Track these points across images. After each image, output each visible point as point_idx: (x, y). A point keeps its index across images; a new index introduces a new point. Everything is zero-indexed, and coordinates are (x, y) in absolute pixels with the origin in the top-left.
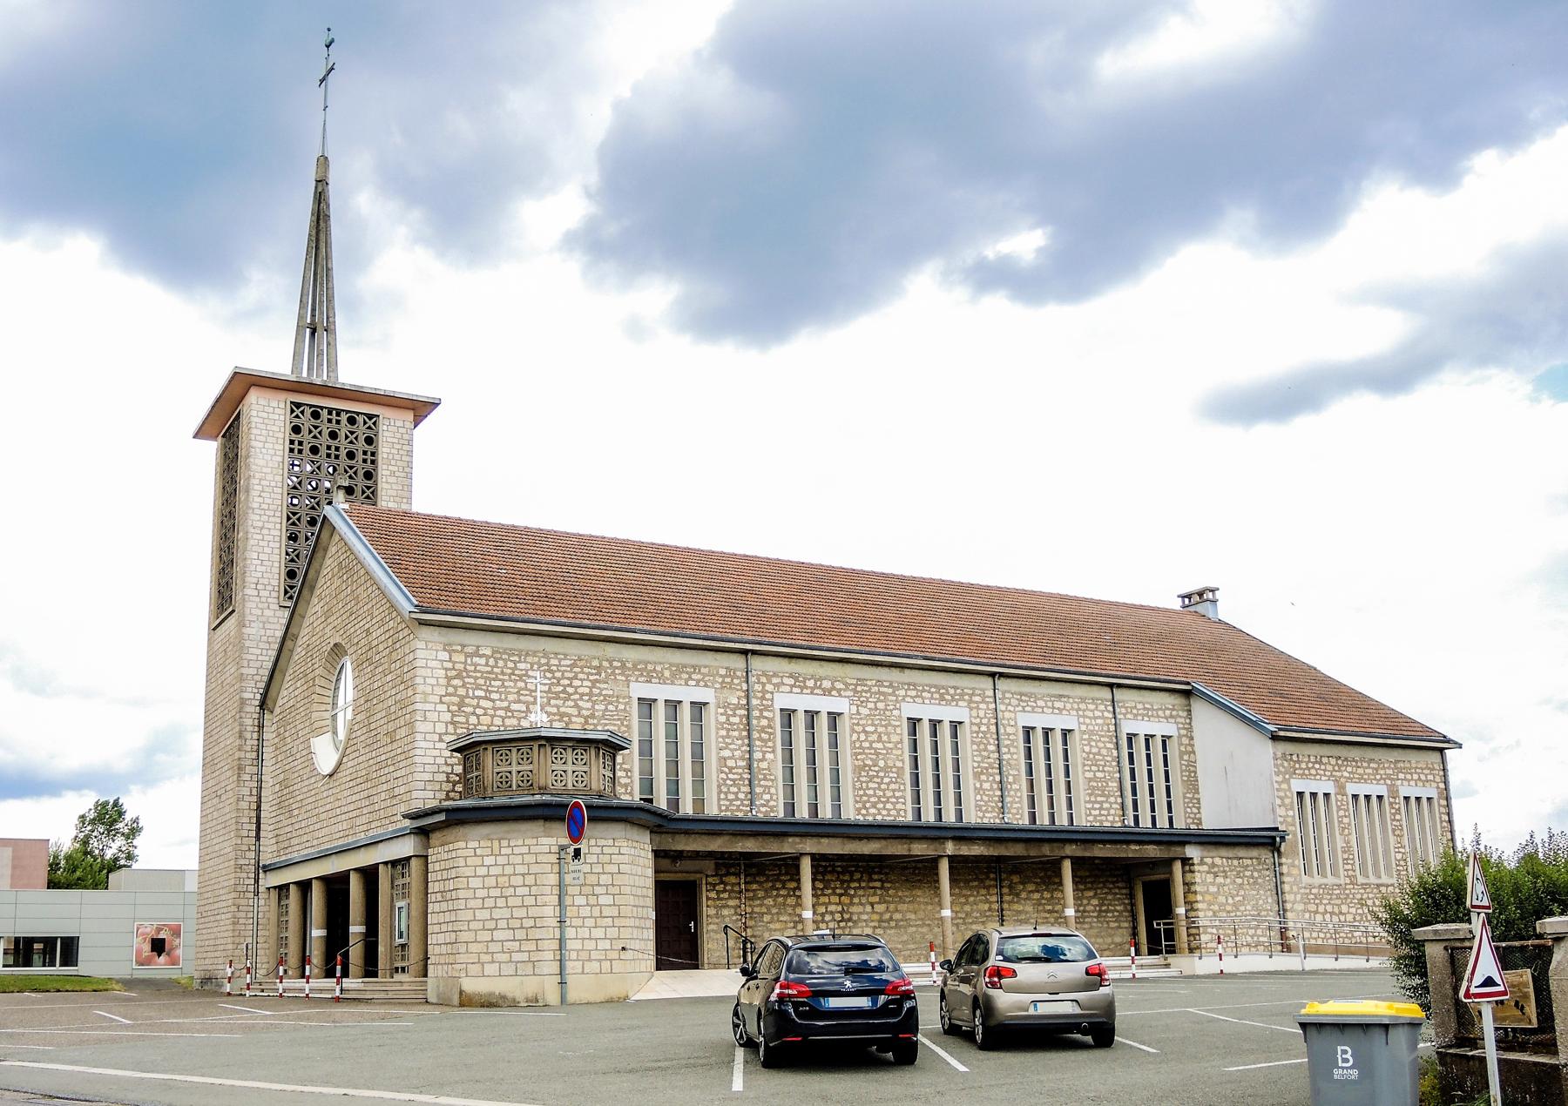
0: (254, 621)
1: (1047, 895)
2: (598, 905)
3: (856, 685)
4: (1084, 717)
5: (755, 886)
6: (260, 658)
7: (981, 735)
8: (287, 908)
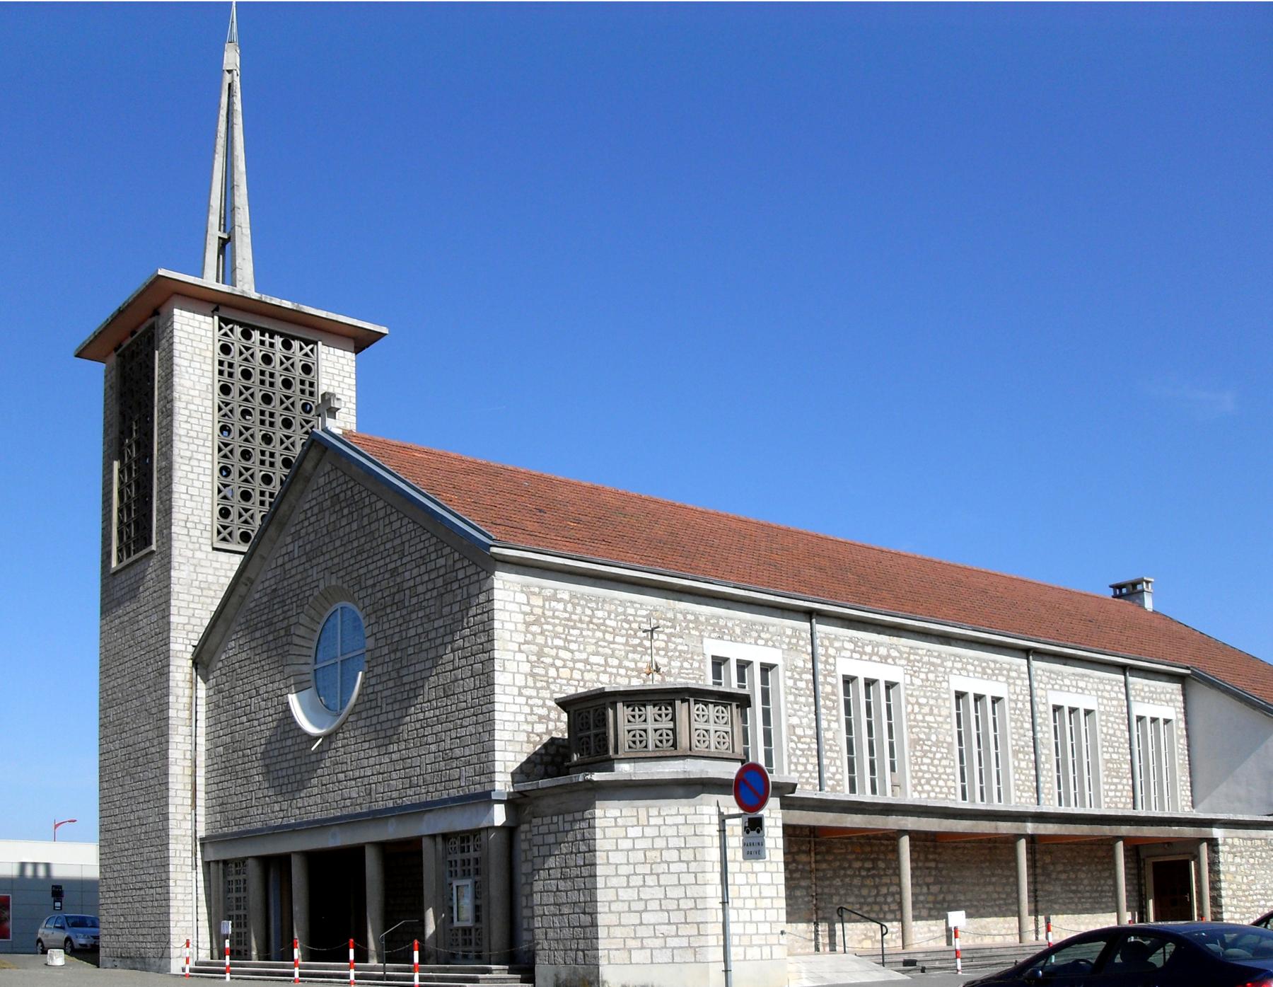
0: (184, 564)
1: (1072, 875)
2: (757, 884)
3: (909, 654)
4: (1103, 697)
5: (824, 866)
6: (192, 605)
7: (1017, 712)
8: (245, 883)
